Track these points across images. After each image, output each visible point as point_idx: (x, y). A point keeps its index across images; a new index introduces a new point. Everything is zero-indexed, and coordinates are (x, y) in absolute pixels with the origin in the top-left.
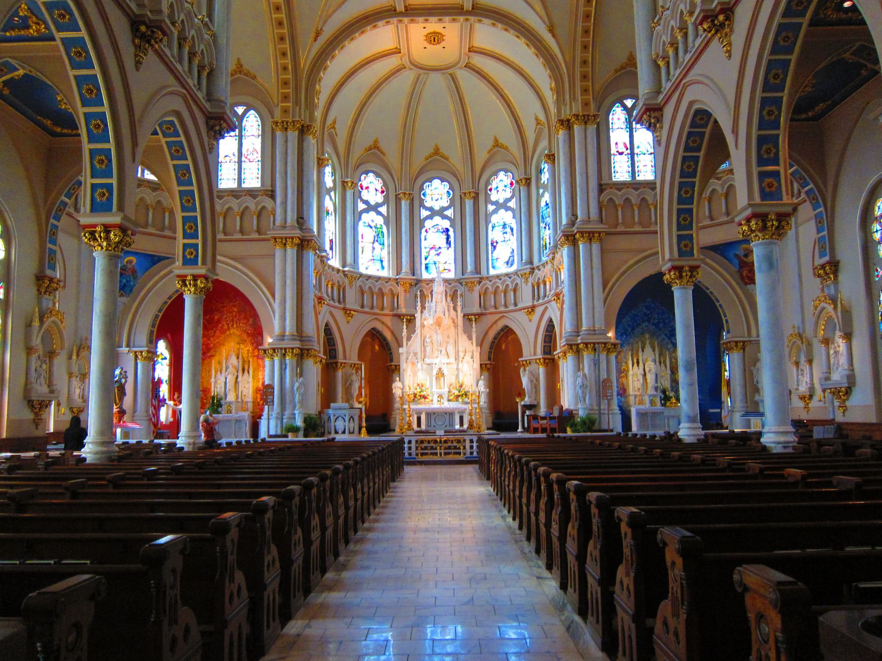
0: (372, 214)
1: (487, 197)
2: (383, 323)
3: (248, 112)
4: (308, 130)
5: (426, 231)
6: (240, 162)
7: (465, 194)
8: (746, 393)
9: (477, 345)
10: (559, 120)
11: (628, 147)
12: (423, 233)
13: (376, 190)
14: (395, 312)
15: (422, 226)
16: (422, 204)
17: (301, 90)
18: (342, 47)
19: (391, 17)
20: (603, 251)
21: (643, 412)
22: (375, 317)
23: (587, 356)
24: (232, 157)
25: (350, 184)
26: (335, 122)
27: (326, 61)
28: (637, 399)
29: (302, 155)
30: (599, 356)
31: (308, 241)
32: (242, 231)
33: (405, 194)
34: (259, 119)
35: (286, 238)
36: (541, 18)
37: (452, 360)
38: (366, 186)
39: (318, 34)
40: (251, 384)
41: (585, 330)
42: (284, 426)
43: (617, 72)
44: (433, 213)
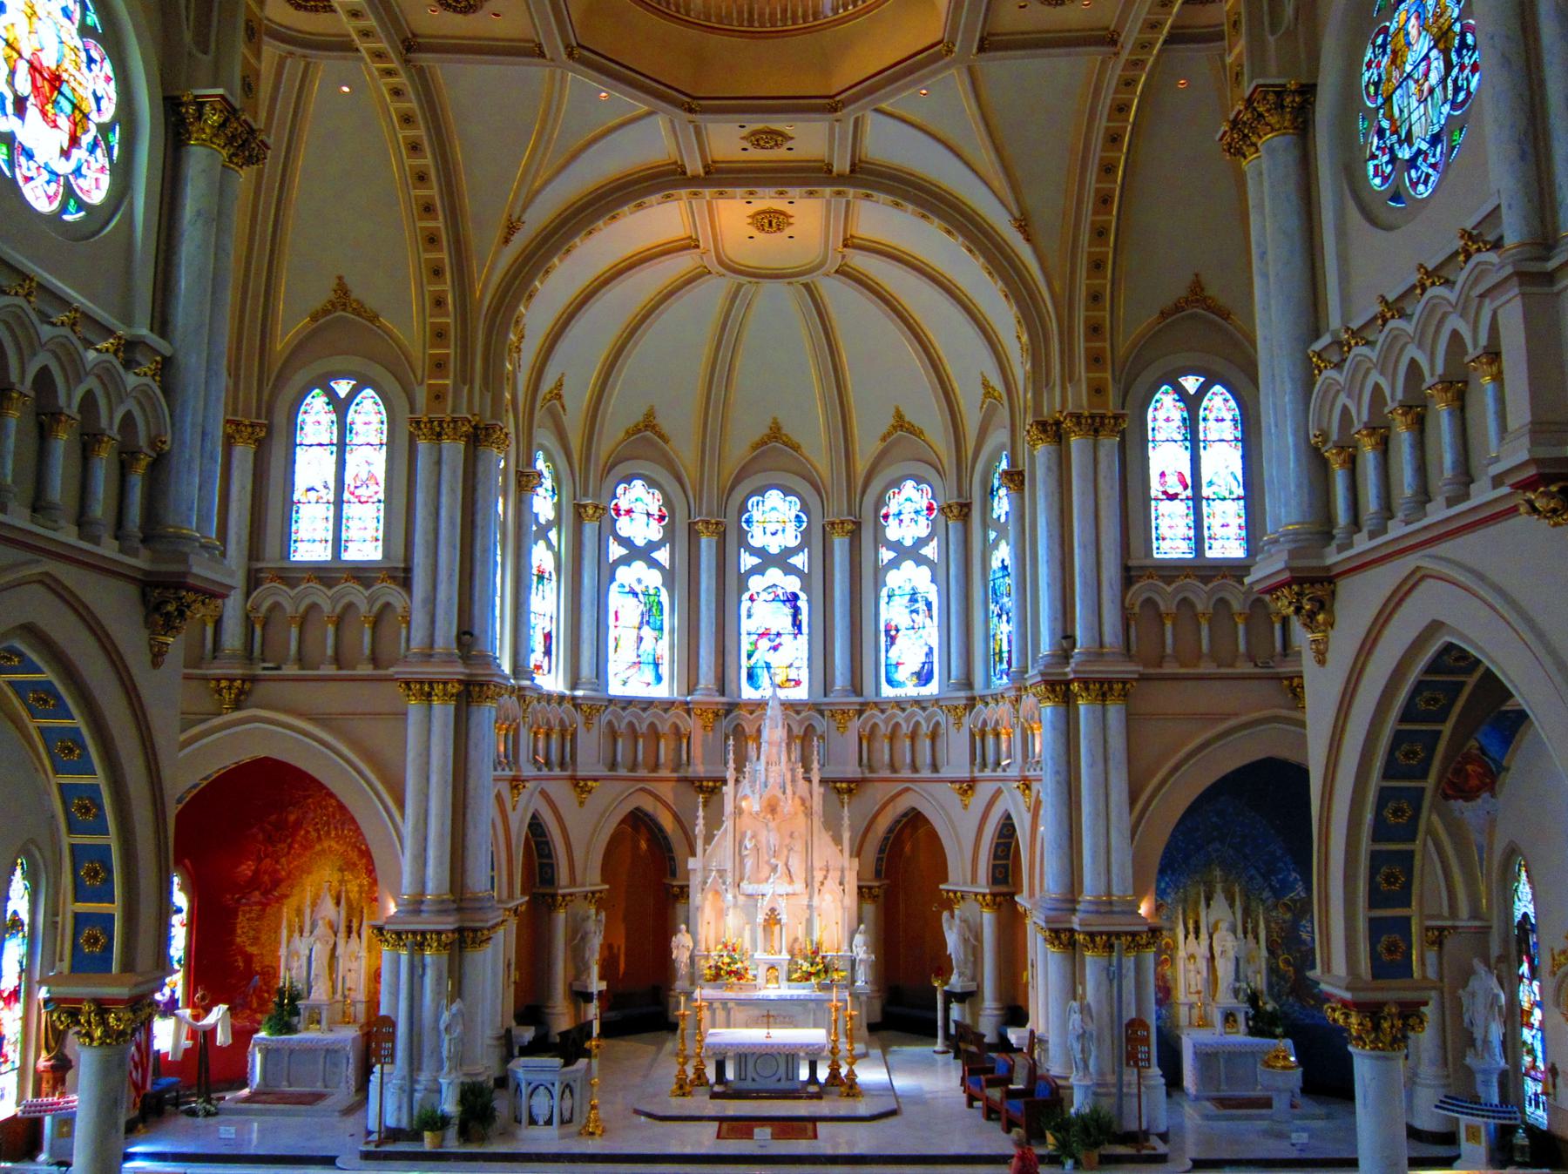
0: (639, 566)
1: (879, 531)
2: (657, 798)
3: (359, 392)
4: (488, 435)
5: (752, 599)
6: (339, 503)
7: (833, 524)
8: (1444, 1042)
9: (851, 856)
10: (1038, 423)
11: (1189, 481)
12: (745, 604)
13: (649, 515)
14: (681, 774)
15: (742, 586)
16: (742, 540)
17: (474, 354)
18: (568, 251)
19: (676, 185)
20: (1130, 718)
21: (1209, 1050)
22: (641, 785)
23: (1092, 962)
24: (323, 492)
25: (590, 512)
26: (560, 385)
27: (517, 306)
28: (1195, 1012)
29: (474, 490)
30: (1120, 960)
31: (481, 685)
32: (338, 660)
33: (707, 523)
34: (382, 408)
35: (431, 684)
36: (1002, 202)
37: (799, 886)
38: (627, 508)
39: (512, 229)
40: (364, 962)
41: (1090, 902)
42: (415, 1112)
43: (1165, 318)
44: (768, 560)
